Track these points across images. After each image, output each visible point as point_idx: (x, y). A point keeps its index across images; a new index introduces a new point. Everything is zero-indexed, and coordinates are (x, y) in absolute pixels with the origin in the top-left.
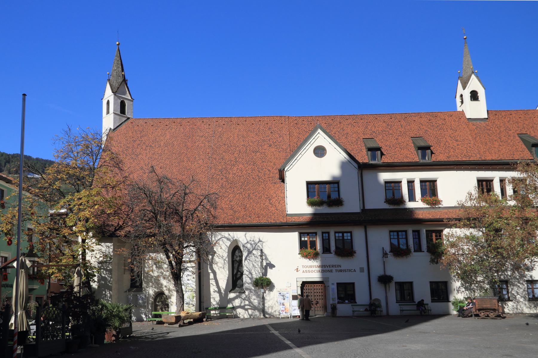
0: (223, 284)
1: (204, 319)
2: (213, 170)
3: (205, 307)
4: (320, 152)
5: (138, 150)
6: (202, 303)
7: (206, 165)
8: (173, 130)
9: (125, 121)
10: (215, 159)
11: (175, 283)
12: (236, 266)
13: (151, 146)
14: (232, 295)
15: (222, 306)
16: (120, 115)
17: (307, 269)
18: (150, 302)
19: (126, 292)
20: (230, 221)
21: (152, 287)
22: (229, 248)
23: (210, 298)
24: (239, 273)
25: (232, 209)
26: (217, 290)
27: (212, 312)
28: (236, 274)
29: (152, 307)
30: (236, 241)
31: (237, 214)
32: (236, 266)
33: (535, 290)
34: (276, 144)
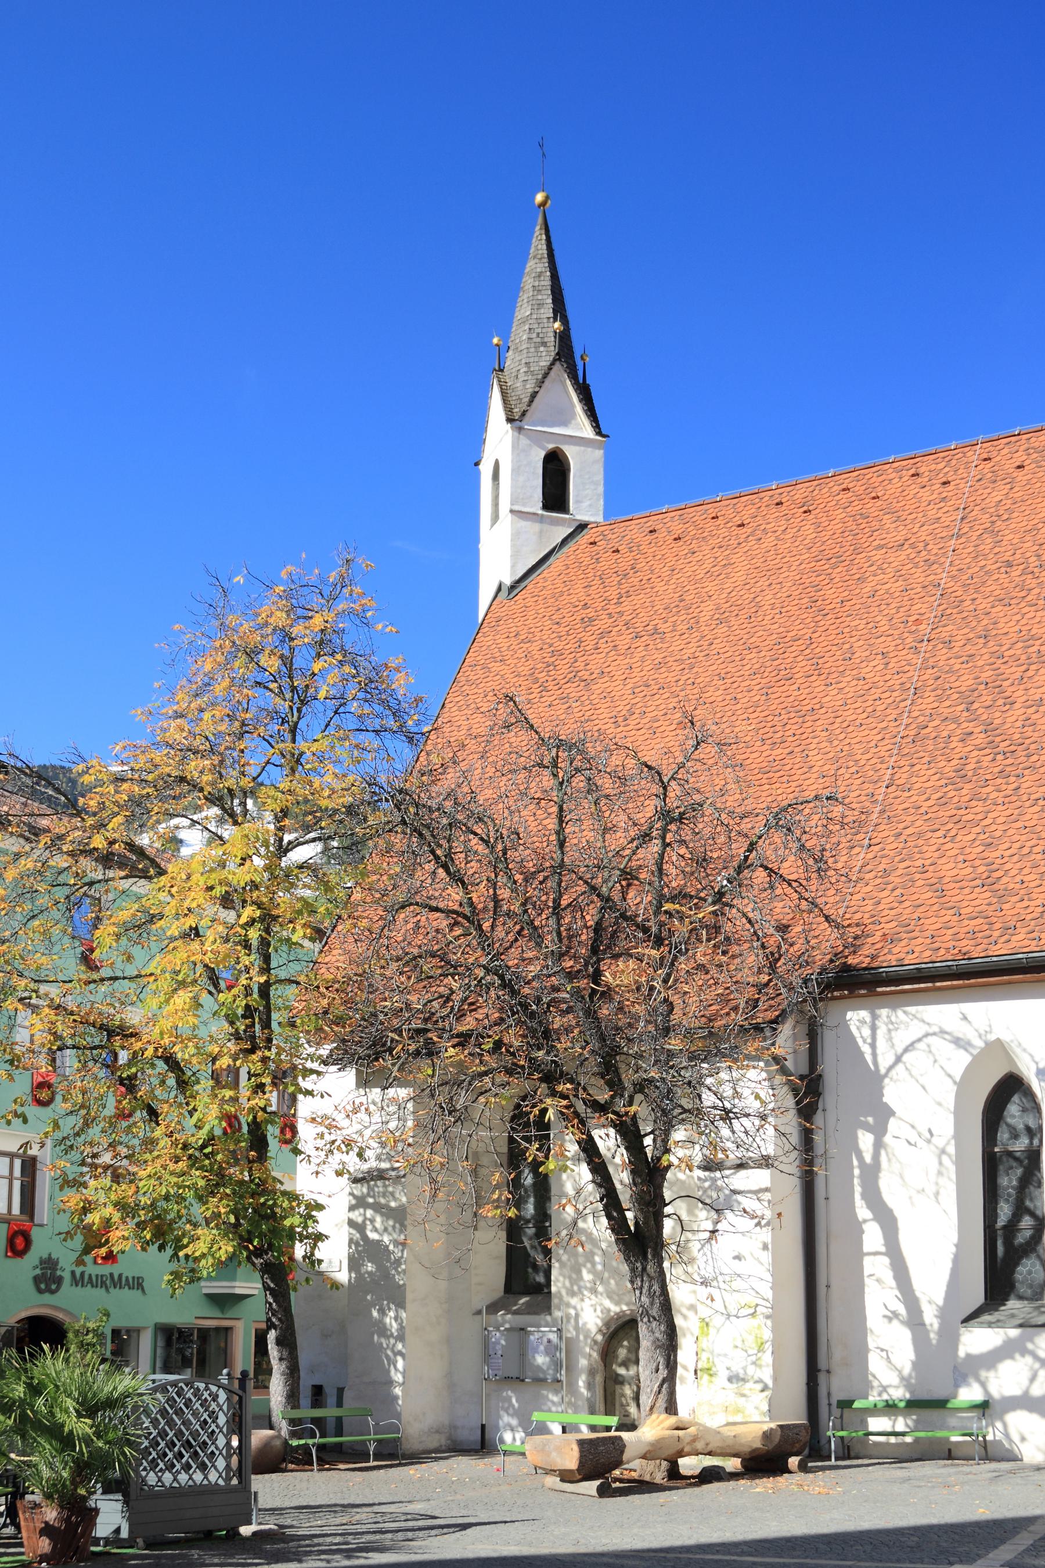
0: (932, 1284)
1: (793, 1461)
2: (928, 701)
3: (837, 1395)
5: (597, 661)
6: (822, 1378)
7: (896, 681)
8: (769, 541)
9: (565, 541)
10: (948, 643)
11: (633, 1270)
12: (1008, 1181)
13: (656, 631)
14: (977, 1340)
15: (925, 1396)
16: (541, 519)
18: (583, 1362)
19: (479, 1312)
20: (966, 945)
21: (594, 1291)
22: (963, 1087)
23: (866, 1350)
24: (1027, 1222)
25: (988, 883)
26: (902, 1310)
27: (877, 1424)
28: (1011, 1227)
29: (590, 1386)
30: (997, 1048)
31: (1011, 908)
32: (1008, 1181)
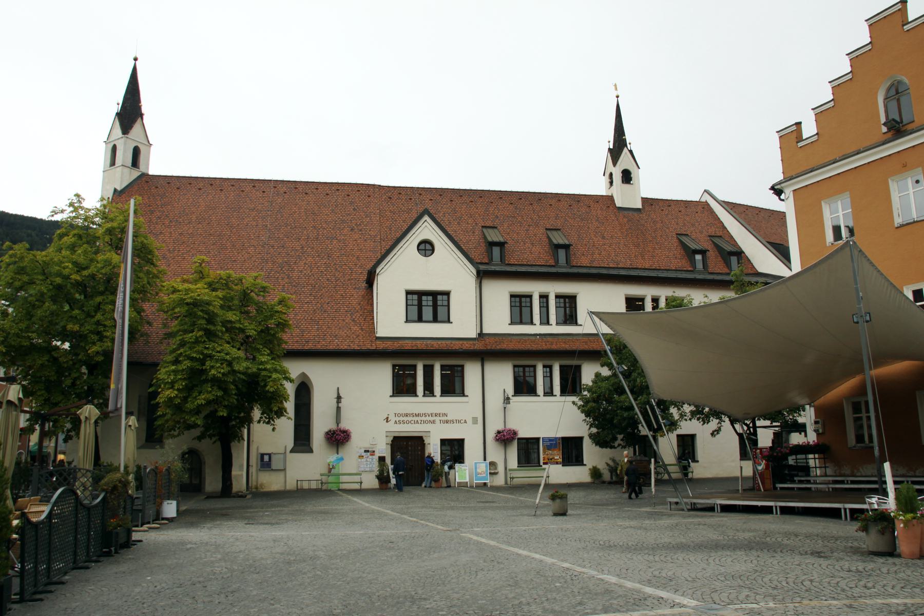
4: (426, 248)
8: (210, 197)
17: (401, 419)
33: (744, 474)
34: (360, 228)
